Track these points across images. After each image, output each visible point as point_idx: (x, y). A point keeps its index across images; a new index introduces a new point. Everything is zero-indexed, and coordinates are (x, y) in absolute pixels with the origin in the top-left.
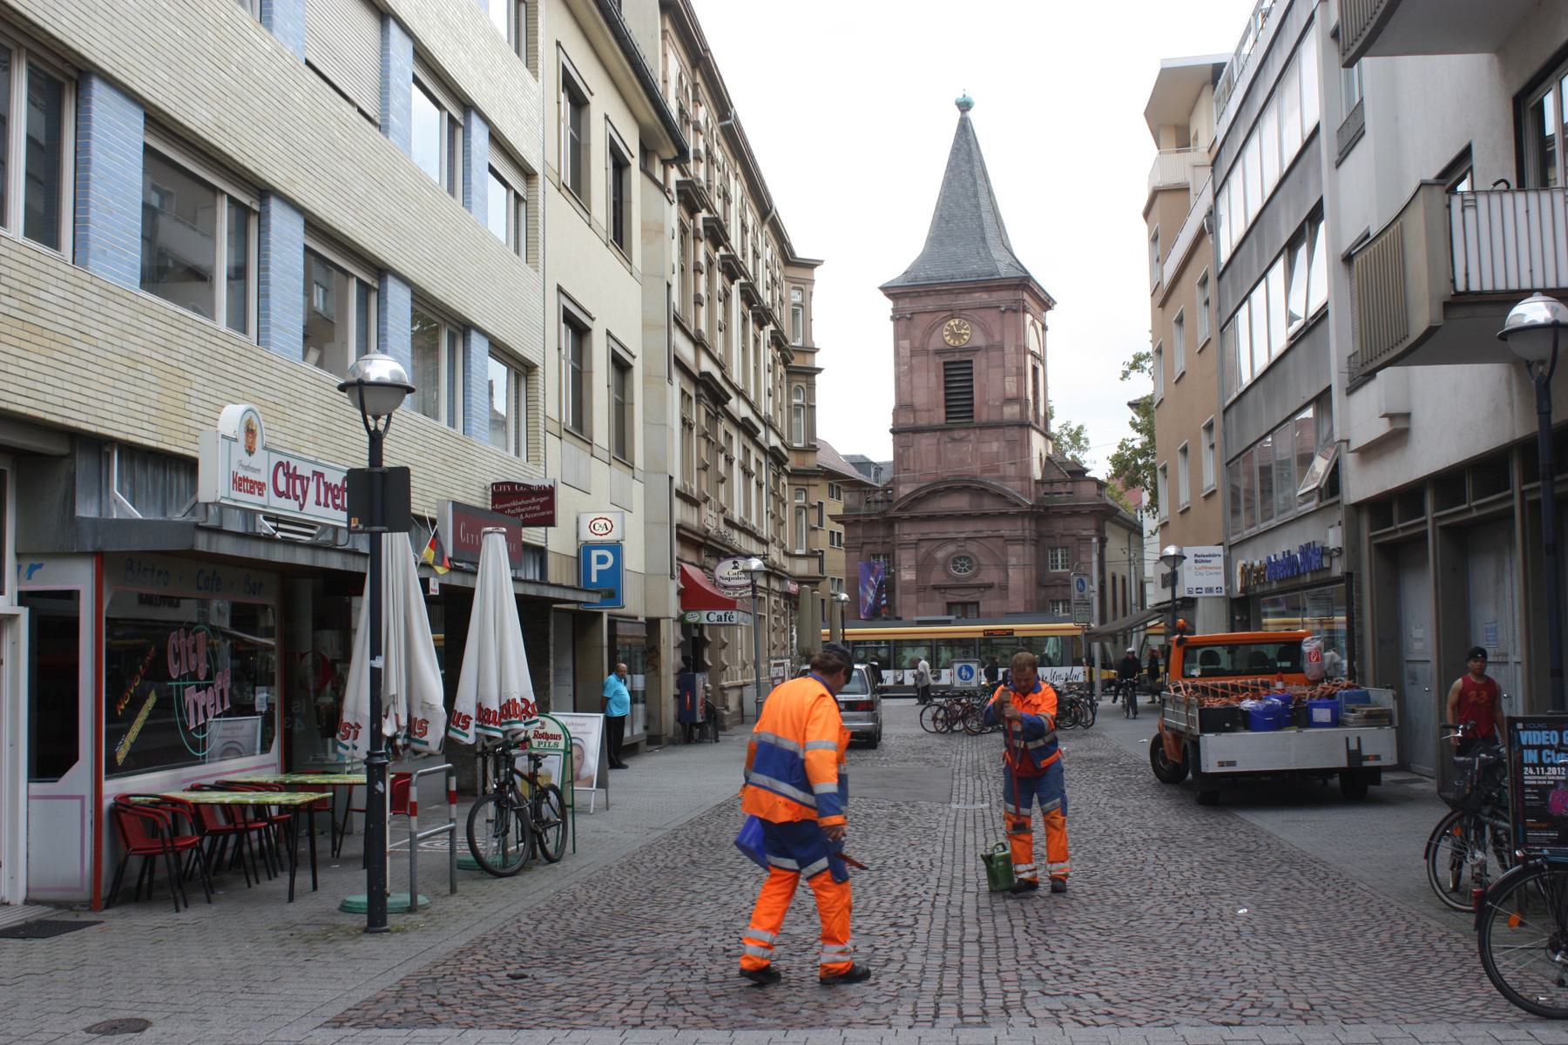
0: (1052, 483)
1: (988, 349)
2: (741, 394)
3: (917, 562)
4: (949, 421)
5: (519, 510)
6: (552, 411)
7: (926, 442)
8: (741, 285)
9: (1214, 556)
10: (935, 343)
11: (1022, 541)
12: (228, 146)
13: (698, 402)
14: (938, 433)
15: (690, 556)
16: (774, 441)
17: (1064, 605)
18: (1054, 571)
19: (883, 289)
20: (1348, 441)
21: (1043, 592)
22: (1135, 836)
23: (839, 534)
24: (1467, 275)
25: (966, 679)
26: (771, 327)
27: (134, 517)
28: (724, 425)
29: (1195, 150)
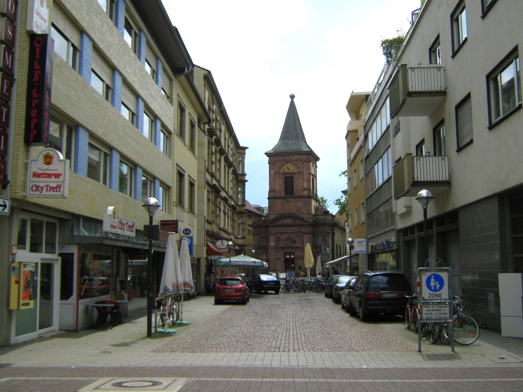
0: (318, 215)
1: (299, 173)
2: (224, 189)
4: (286, 195)
5: (168, 229)
6: (175, 199)
7: (279, 202)
8: (224, 156)
9: (363, 241)
10: (282, 171)
11: (308, 233)
12: (105, 138)
13: (212, 193)
14: (283, 199)
15: (209, 240)
16: (233, 203)
18: (318, 243)
19: (265, 153)
20: (397, 212)
22: (334, 319)
23: (251, 230)
24: (417, 177)
25: (435, 290)
26: (232, 168)
27: (85, 235)
28: (219, 199)
29: (361, 120)
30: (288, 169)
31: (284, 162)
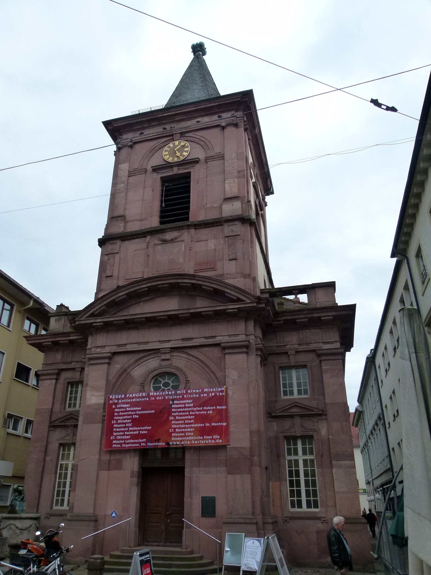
3: (107, 380)
17: (303, 443)
19: (107, 124)
21: (275, 426)
31: (163, 140)
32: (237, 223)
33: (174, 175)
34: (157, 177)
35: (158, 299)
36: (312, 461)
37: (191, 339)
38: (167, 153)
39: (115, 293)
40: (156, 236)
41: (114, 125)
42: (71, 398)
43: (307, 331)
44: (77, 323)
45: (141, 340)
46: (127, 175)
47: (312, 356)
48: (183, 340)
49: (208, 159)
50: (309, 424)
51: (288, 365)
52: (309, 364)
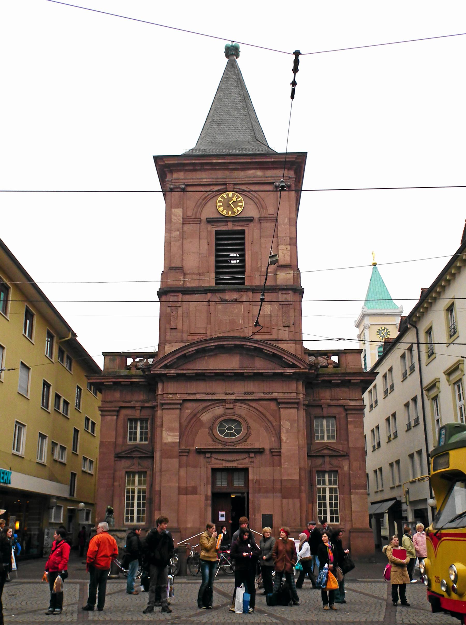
3: (180, 424)
10: (208, 213)
30: (228, 207)
32: (290, 292)
33: (228, 230)
34: (213, 229)
35: (221, 355)
36: (335, 489)
37: (252, 393)
38: (221, 204)
39: (186, 348)
40: (217, 294)
41: (166, 162)
42: (131, 433)
43: (338, 389)
44: (152, 372)
45: (208, 391)
46: (182, 223)
47: (340, 410)
48: (245, 393)
49: (262, 220)
50: (335, 462)
51: (322, 415)
52: (337, 416)
